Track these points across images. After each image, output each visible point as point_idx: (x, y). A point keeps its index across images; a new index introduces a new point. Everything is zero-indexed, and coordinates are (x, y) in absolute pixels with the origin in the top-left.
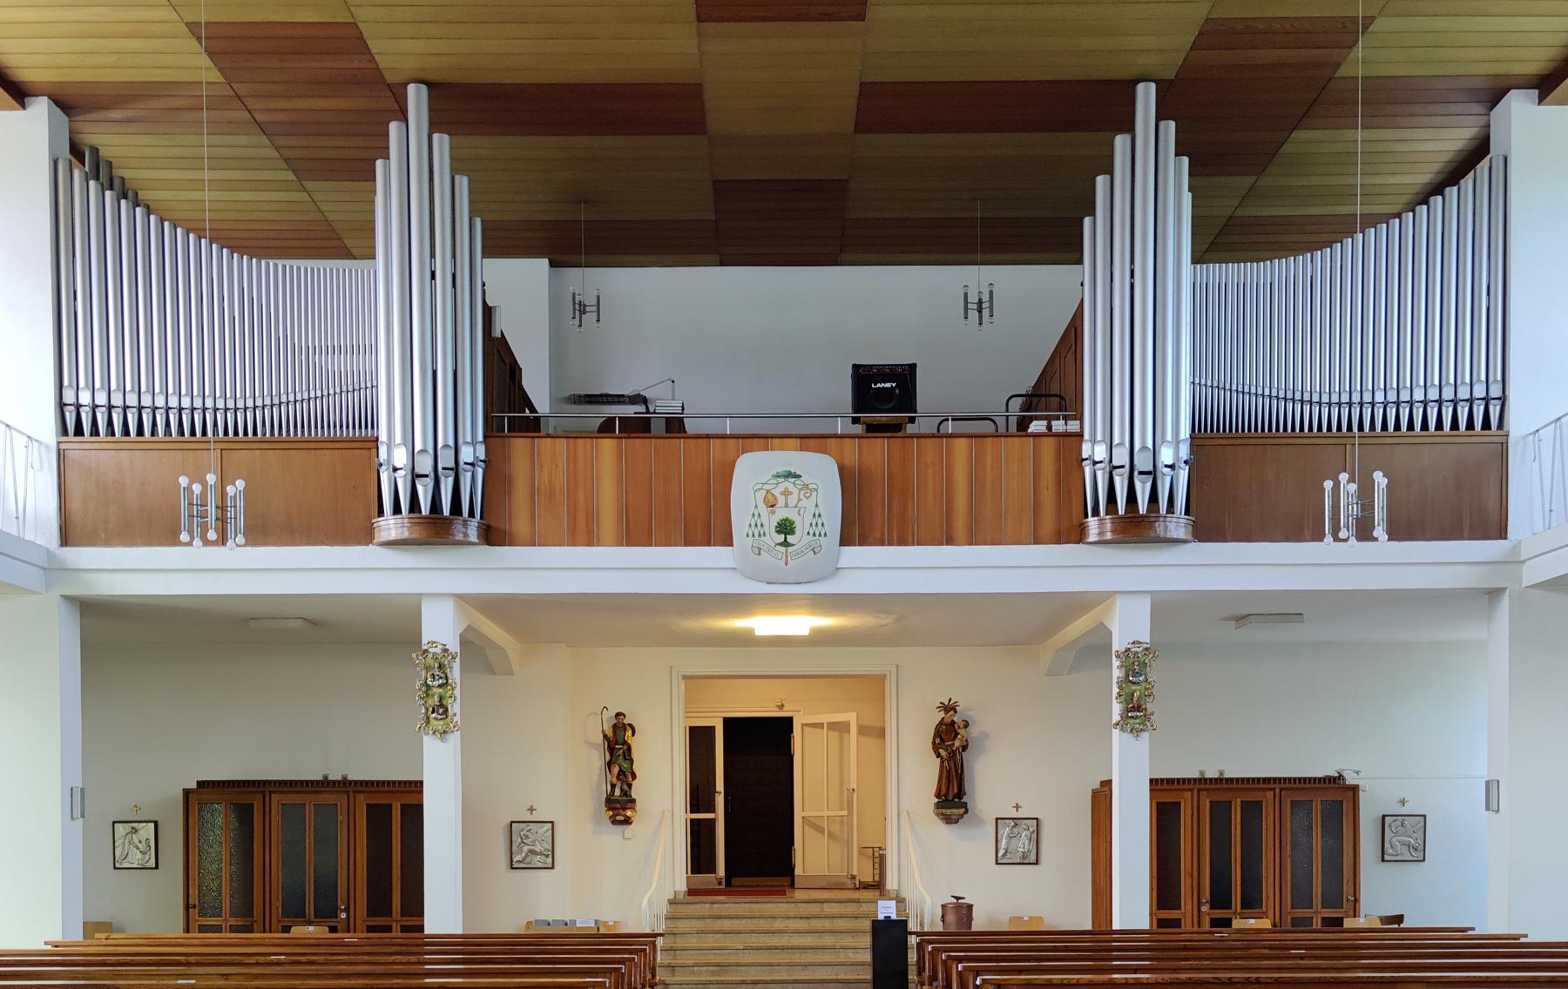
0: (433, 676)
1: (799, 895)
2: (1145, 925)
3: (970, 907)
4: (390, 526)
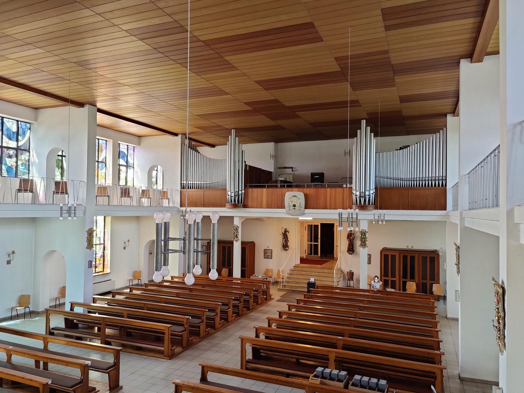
0: (235, 231)
4: (228, 205)
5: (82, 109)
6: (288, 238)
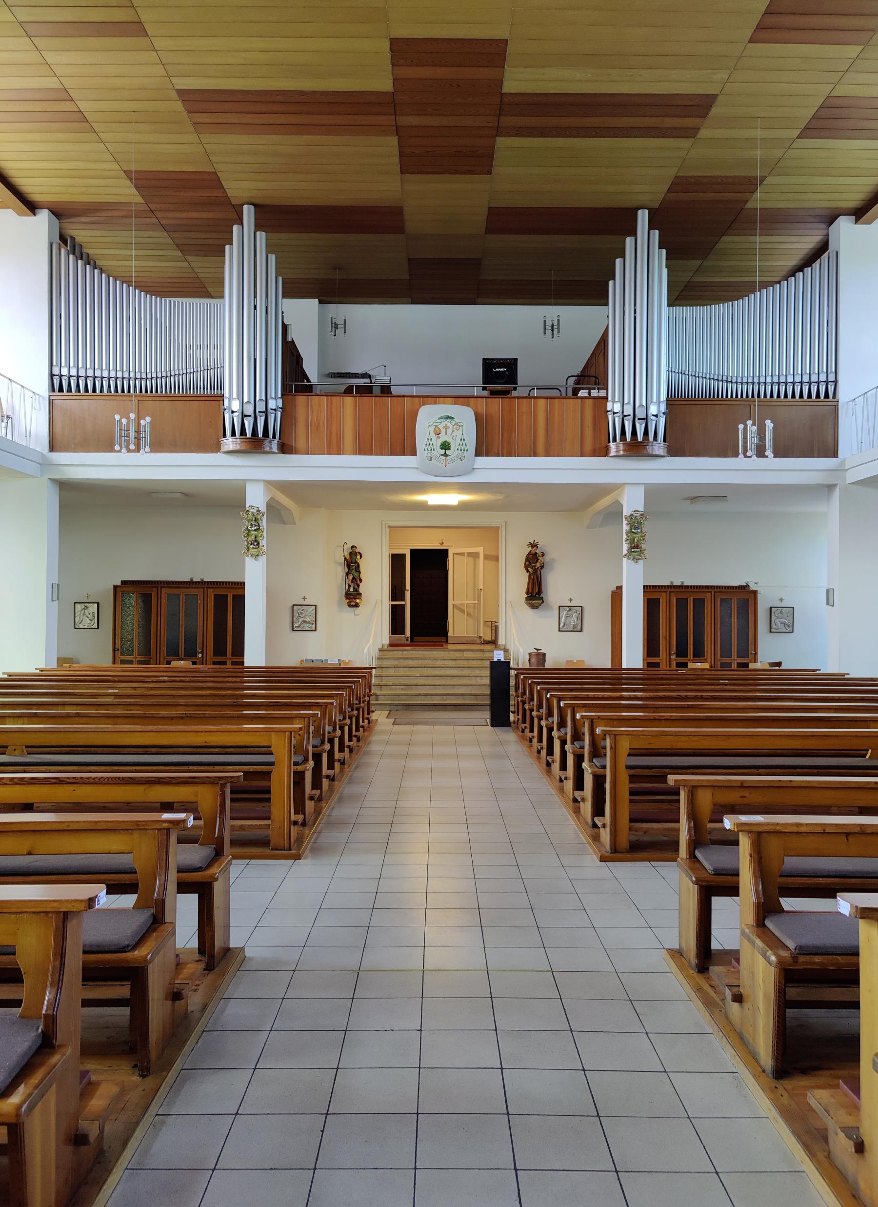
1: (450, 647)
2: (640, 666)
3: (544, 654)
5: (30, 219)
6: (360, 572)
